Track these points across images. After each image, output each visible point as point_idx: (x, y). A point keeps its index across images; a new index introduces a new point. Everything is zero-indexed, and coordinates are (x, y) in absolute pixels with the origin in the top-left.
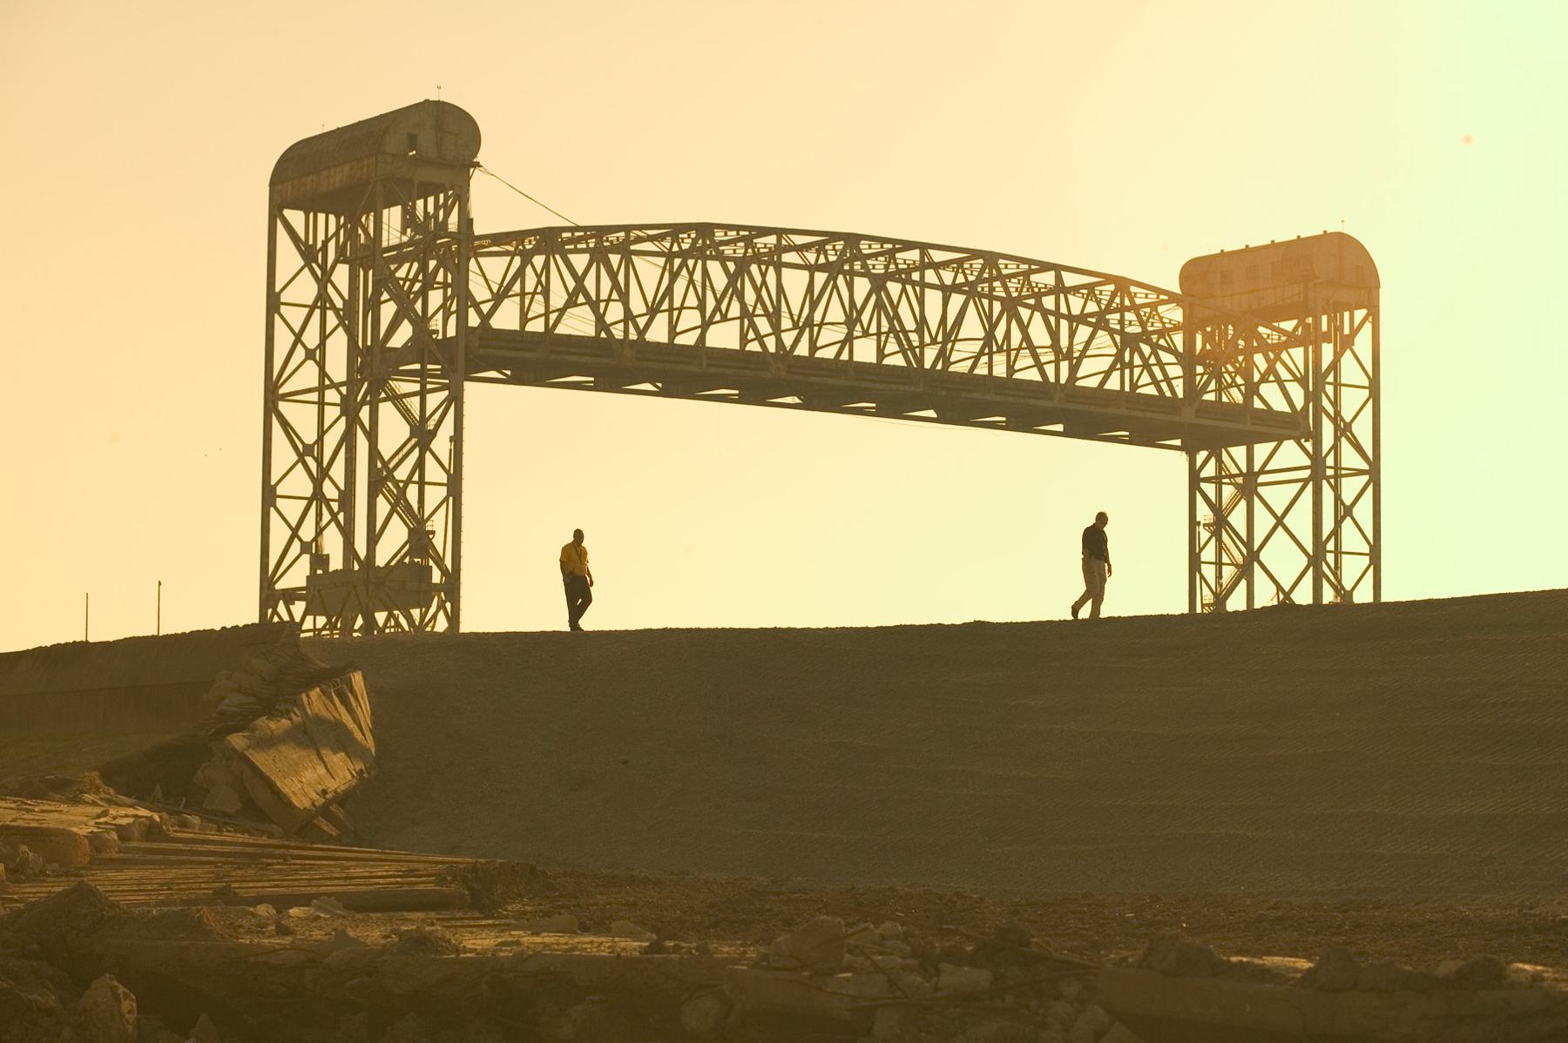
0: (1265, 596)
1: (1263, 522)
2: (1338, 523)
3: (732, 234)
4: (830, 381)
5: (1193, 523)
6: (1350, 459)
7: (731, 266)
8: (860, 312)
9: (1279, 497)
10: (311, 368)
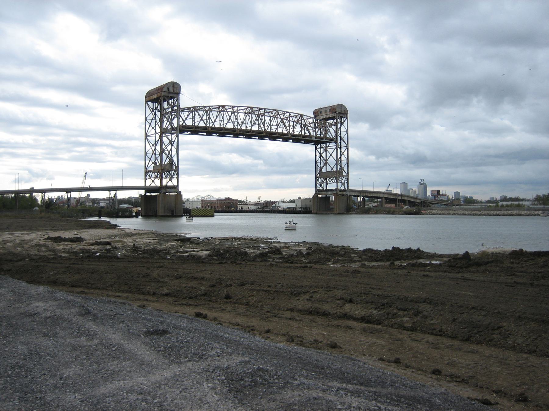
0: (329, 169)
1: (328, 155)
2: (341, 156)
3: (229, 107)
4: (248, 133)
5: (316, 156)
6: (343, 144)
7: (256, 116)
8: (279, 124)
9: (330, 151)
10: (153, 131)
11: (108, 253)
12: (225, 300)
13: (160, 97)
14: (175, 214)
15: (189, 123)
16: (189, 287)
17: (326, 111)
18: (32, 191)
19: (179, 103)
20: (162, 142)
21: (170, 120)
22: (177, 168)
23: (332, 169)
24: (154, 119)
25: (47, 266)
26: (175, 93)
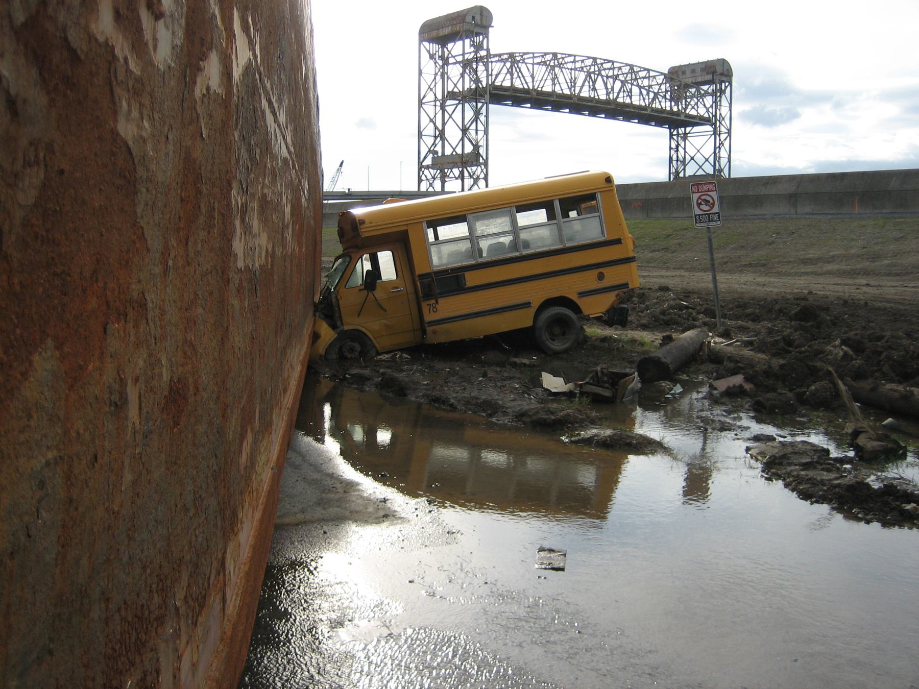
0: (448, 151)
17: (693, 71)
23: (454, 150)
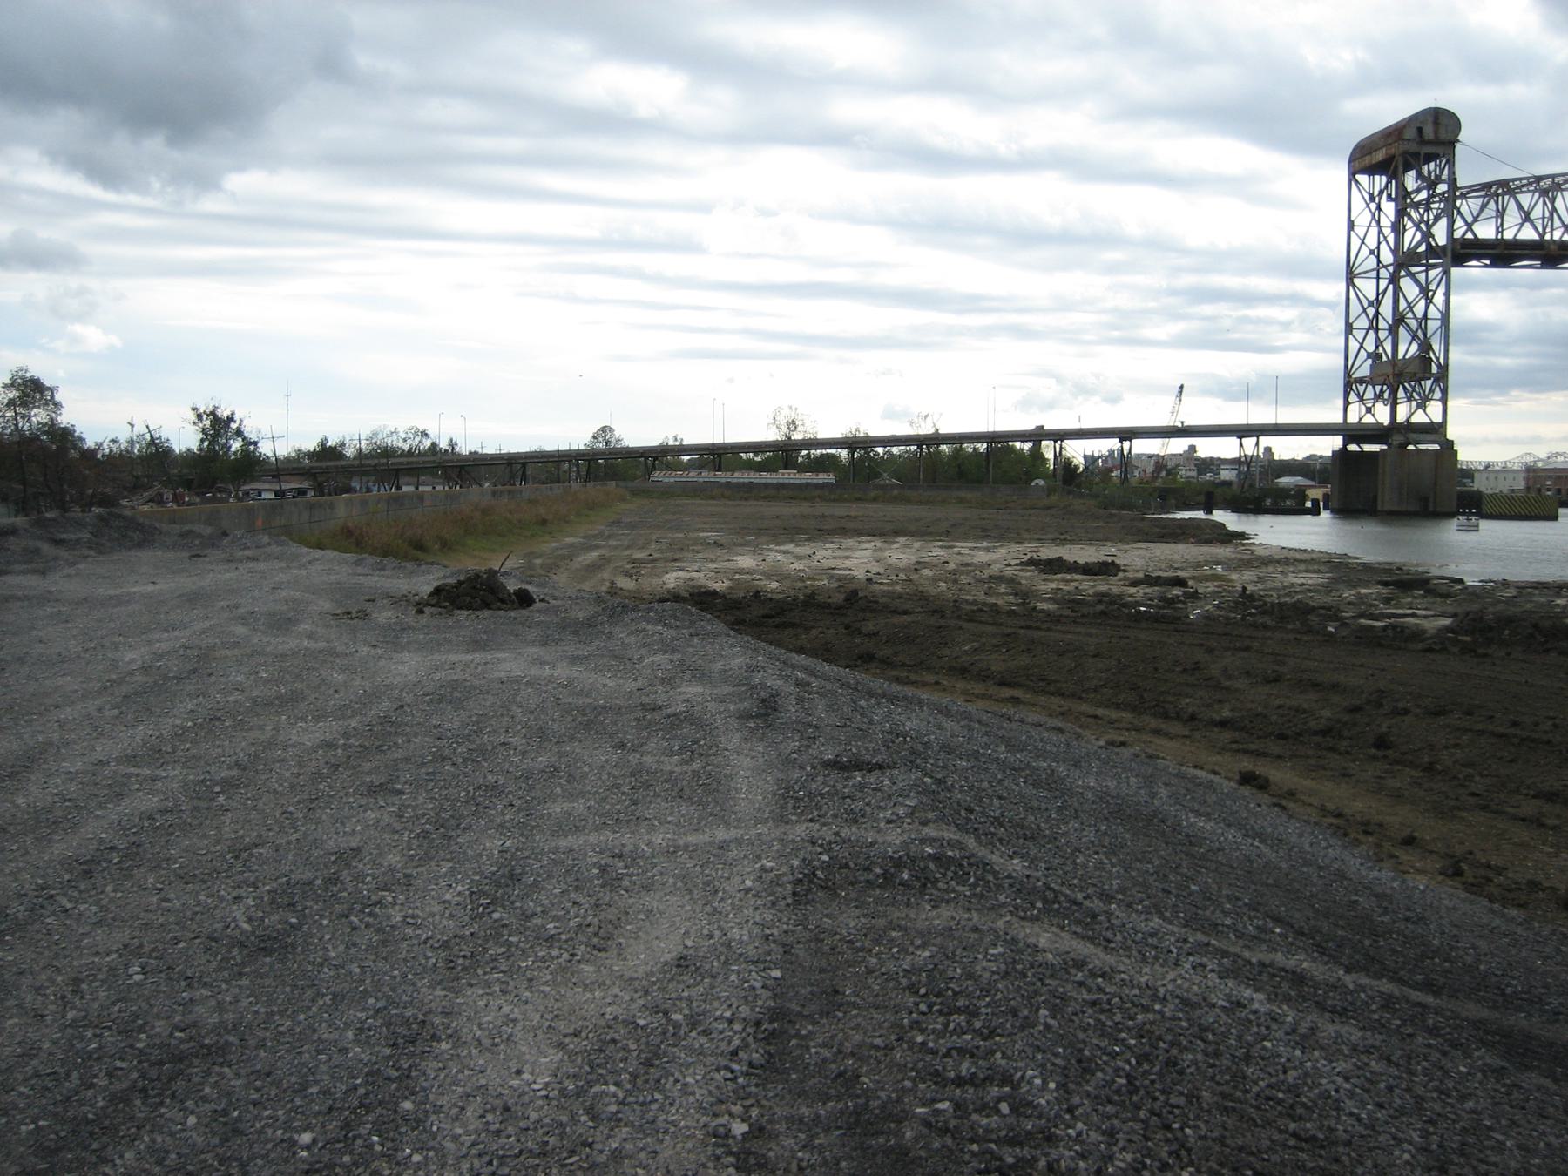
10: (1373, 259)
11: (1164, 608)
12: (1373, 751)
13: (1394, 157)
14: (1431, 509)
15: (1485, 231)
16: (1290, 709)
18: (1038, 435)
19: (1452, 173)
20: (1398, 291)
21: (1423, 226)
22: (1444, 369)
24: (1374, 223)
25: (961, 628)
26: (1443, 143)
